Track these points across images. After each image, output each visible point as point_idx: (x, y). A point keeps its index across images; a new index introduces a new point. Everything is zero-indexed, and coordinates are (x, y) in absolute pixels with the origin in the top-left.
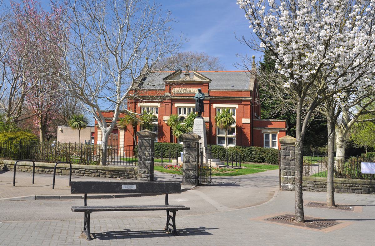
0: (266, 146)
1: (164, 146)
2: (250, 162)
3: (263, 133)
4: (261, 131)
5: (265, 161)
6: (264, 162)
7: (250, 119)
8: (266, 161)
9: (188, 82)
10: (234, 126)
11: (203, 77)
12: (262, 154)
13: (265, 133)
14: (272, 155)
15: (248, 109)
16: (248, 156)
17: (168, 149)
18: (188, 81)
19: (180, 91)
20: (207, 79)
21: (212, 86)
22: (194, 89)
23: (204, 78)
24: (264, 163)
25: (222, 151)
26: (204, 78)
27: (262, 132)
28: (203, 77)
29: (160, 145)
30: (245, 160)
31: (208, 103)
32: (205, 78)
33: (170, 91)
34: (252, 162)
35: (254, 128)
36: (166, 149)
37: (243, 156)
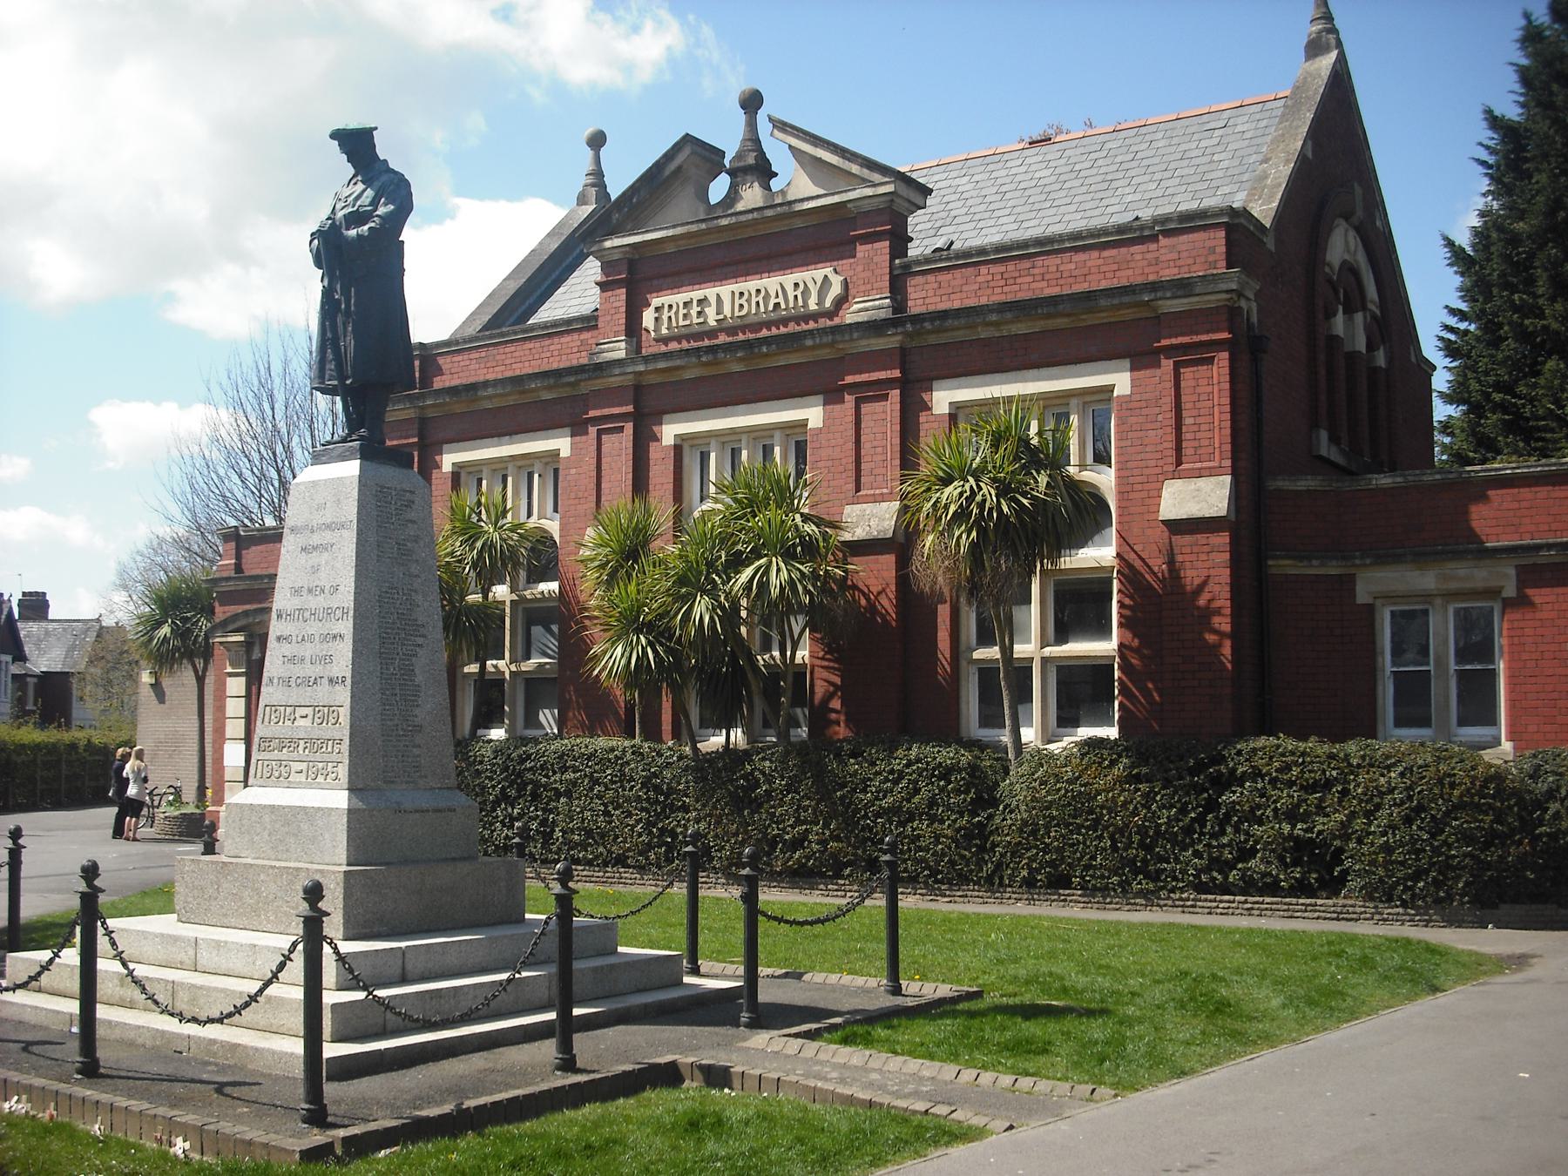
0: (1399, 723)
1: (542, 768)
2: (1201, 888)
3: (1370, 609)
4: (1347, 583)
5: (1342, 880)
6: (1333, 886)
7: (1228, 478)
8: (1354, 883)
9: (750, 233)
10: (1099, 554)
11: (846, 165)
12: (1320, 809)
13: (1389, 597)
14: (1408, 821)
15: (1211, 386)
16: (1188, 831)
17: (568, 794)
18: (743, 218)
19: (695, 310)
20: (877, 177)
21: (926, 233)
22: (789, 279)
23: (855, 169)
24: (1336, 894)
25: (958, 792)
26: (855, 169)
27: (1362, 597)
28: (846, 165)
29: (522, 761)
30: (1155, 877)
31: (890, 383)
32: (866, 173)
33: (633, 328)
34: (1225, 889)
35: (1282, 566)
36: (558, 795)
37: (1142, 831)
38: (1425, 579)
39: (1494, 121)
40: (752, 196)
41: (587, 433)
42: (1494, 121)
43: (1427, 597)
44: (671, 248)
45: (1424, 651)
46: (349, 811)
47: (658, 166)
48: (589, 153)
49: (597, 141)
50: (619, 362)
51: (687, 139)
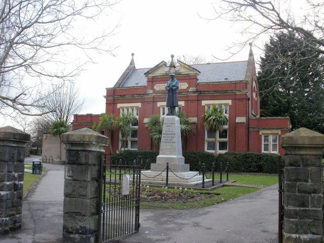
13: (263, 134)
38: (269, 132)
39: (262, 58)
40: (173, 70)
41: (76, 116)
42: (262, 58)
43: (269, 134)
44: (159, 77)
45: (268, 141)
46: (66, 213)
47: (158, 65)
48: (131, 56)
49: (133, 55)
50: (151, 94)
51: (163, 61)
